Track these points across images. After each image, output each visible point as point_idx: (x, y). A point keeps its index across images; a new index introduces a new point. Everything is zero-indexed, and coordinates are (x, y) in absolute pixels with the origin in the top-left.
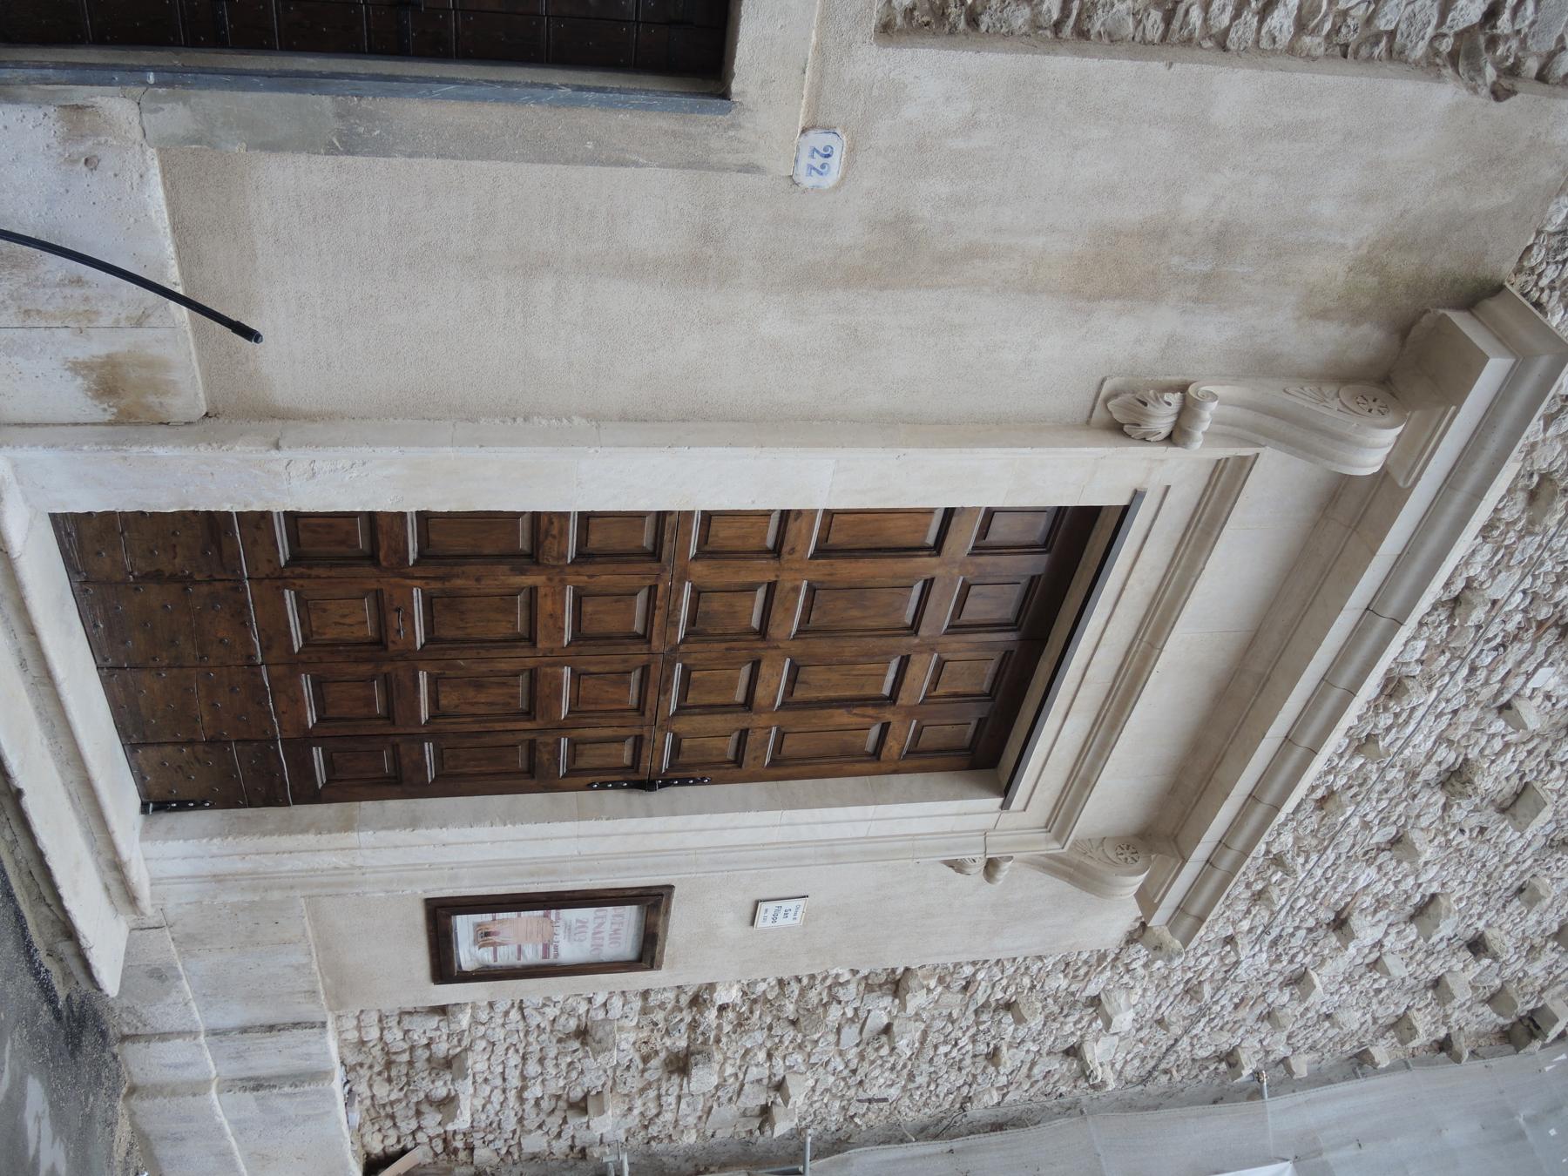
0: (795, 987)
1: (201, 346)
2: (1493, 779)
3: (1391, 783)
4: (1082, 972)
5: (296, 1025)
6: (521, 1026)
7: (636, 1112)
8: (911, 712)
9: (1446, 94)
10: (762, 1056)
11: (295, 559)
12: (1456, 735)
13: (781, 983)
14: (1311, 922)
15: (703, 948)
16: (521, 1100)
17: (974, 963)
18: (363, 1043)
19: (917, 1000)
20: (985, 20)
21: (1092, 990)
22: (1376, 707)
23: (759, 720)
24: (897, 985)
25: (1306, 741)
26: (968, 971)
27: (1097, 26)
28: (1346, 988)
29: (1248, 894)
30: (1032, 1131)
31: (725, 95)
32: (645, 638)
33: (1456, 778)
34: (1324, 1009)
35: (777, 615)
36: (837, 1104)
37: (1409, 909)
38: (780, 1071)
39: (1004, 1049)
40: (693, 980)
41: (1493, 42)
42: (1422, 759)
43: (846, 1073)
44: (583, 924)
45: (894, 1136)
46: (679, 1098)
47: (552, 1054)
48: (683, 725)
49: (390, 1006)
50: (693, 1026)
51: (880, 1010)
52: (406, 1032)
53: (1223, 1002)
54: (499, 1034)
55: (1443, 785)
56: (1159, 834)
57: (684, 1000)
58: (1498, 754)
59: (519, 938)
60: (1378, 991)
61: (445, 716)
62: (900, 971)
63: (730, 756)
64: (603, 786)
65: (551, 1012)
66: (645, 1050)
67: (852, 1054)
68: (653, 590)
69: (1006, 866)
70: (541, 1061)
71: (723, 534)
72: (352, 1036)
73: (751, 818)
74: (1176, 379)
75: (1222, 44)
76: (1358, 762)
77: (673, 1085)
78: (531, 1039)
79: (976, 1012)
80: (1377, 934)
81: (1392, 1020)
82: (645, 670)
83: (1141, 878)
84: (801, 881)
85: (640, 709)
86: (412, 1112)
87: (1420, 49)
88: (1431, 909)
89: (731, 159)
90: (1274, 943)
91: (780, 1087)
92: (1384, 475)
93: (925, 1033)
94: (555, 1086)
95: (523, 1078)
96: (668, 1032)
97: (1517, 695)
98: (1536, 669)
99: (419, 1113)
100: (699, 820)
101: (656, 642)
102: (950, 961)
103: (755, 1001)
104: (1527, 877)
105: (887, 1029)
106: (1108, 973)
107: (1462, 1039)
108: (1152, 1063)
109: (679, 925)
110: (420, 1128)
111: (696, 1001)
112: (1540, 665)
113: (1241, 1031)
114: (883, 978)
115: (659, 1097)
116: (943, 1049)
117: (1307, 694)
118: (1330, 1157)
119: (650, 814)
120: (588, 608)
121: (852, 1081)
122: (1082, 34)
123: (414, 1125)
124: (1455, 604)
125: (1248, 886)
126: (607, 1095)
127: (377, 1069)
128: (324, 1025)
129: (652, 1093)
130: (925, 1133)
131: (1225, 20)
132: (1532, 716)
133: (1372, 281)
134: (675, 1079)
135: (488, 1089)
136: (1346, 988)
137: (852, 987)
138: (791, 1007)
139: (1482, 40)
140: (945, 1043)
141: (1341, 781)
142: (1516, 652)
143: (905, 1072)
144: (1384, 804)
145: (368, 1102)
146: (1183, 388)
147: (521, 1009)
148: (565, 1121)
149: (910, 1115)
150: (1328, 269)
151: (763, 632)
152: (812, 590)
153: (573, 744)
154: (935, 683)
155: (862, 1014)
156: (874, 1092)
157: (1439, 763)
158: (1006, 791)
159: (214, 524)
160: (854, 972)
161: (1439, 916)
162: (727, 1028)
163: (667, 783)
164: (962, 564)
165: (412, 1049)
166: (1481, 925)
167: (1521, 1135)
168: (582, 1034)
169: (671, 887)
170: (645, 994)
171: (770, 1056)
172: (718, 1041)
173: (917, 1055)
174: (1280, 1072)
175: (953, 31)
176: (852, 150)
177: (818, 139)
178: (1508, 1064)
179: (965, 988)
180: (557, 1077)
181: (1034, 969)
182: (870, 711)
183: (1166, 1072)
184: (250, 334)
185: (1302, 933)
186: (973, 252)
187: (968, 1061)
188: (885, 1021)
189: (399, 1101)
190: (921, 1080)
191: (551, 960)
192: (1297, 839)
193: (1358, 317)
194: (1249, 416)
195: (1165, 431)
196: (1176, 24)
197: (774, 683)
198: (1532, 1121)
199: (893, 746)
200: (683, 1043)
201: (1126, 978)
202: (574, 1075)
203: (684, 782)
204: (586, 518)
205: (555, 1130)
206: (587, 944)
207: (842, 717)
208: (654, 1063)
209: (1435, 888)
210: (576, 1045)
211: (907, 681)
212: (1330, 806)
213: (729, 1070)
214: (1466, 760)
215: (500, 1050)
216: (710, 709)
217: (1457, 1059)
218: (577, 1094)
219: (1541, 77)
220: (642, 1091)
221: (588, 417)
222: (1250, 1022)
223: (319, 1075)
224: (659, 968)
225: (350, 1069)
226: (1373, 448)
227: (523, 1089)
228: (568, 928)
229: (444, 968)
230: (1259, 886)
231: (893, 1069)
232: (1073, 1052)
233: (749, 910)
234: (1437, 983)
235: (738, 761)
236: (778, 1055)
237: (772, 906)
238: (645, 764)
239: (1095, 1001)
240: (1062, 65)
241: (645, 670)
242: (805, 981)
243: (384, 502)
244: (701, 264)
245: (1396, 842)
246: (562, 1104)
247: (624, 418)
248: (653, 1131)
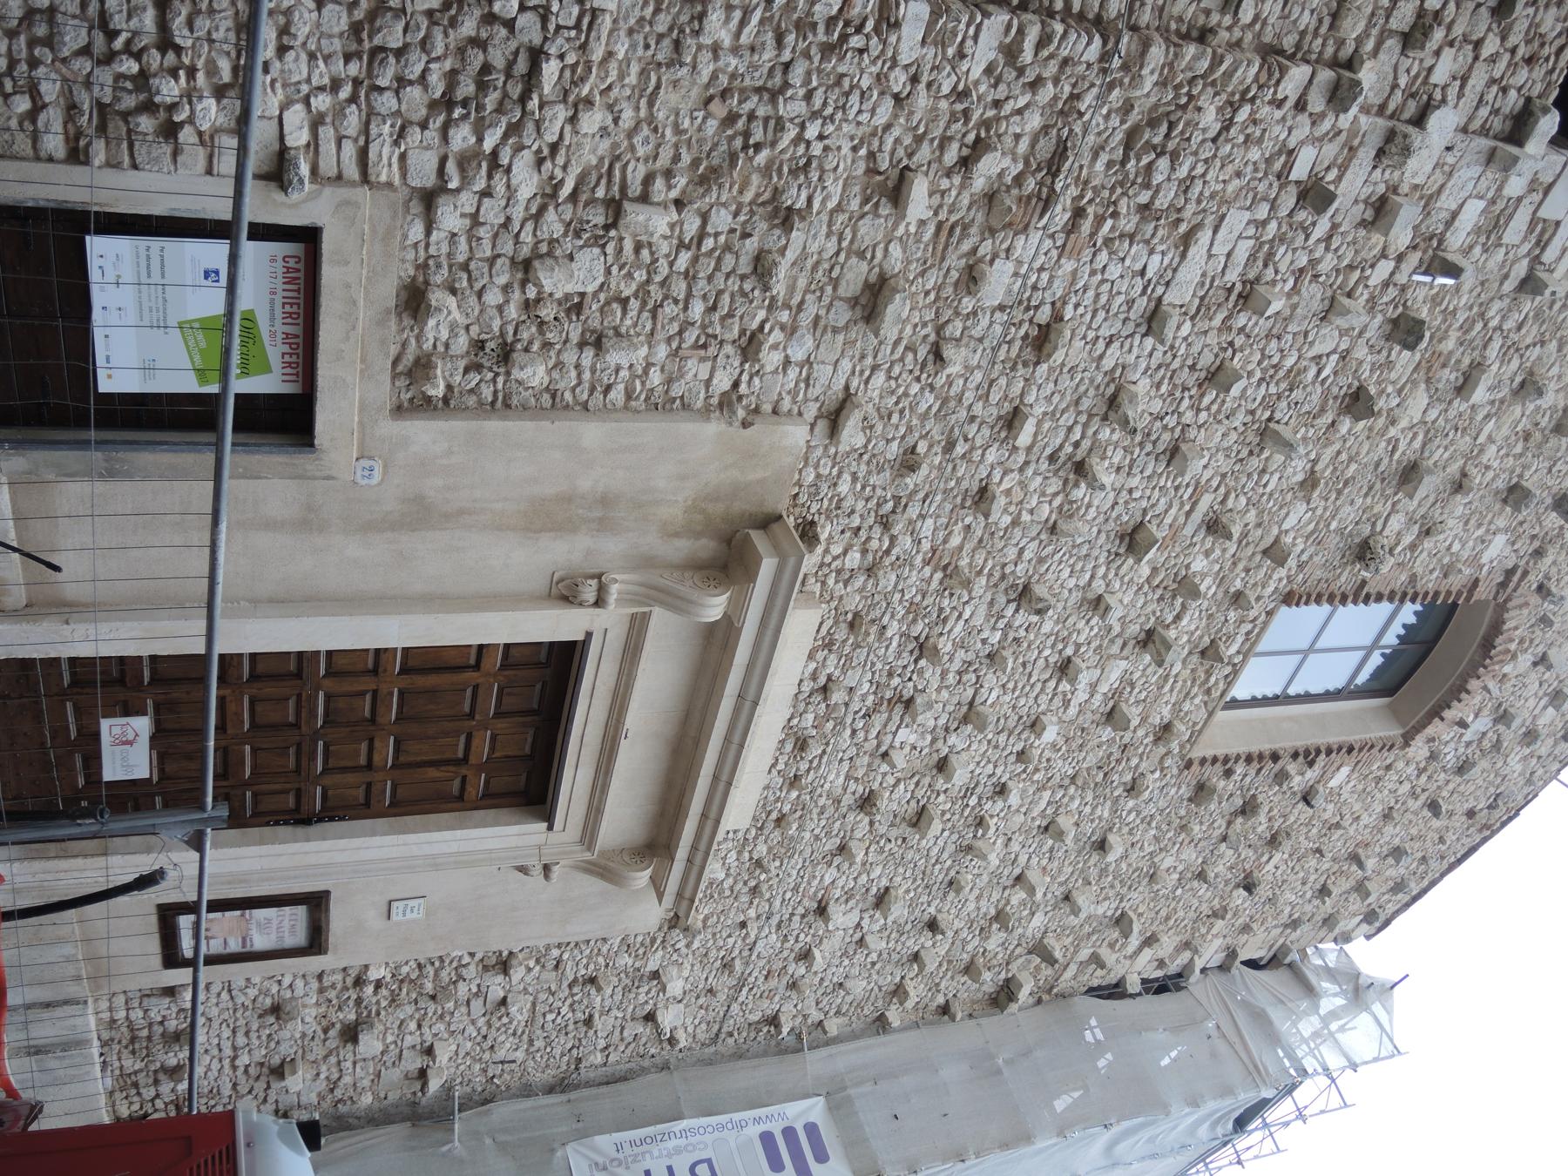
0: (430, 970)
1: (25, 569)
2: (895, 801)
3: (823, 807)
4: (641, 952)
5: (66, 1002)
6: (230, 1005)
7: (322, 1076)
8: (480, 768)
9: (714, 428)
10: (413, 1026)
11: (73, 683)
12: (860, 773)
13: (420, 966)
14: (801, 910)
15: (360, 938)
16: (234, 1068)
17: (559, 946)
18: (113, 1021)
19: (517, 973)
20: (452, 403)
21: (652, 965)
23: (378, 776)
24: (504, 965)
25: (724, 778)
26: (555, 953)
27: (515, 401)
28: (846, 962)
29: (746, 889)
30: (632, 1084)
31: (312, 445)
32: (297, 725)
33: (867, 803)
34: (835, 980)
35: (381, 710)
36: (478, 1067)
37: (871, 899)
38: (429, 1038)
39: (597, 1016)
40: (356, 962)
41: (740, 398)
42: (840, 790)
43: (479, 1039)
44: (269, 921)
45: (527, 1091)
46: (355, 1063)
47: (255, 1027)
48: (328, 780)
49: (133, 985)
50: (359, 1001)
51: (496, 986)
52: (146, 1011)
53: (755, 974)
54: (214, 1012)
55: (861, 807)
56: (656, 845)
57: (349, 981)
58: (894, 786)
59: (223, 932)
60: (873, 964)
61: (169, 778)
62: (505, 954)
63: (362, 801)
64: (277, 823)
65: (252, 992)
66: (324, 1023)
67: (481, 1022)
68: (299, 696)
69: (555, 868)
70: (247, 1034)
71: (340, 662)
72: (106, 1016)
73: (377, 840)
74: (597, 571)
75: (585, 406)
76: (794, 794)
77: (347, 1052)
78: (239, 1014)
79: (570, 986)
80: (854, 918)
81: (893, 988)
82: (299, 745)
83: (648, 872)
84: (417, 885)
85: (298, 770)
86: (151, 1081)
87: (699, 404)
89: (318, 474)
90: (779, 926)
91: (429, 1051)
92: (726, 616)
93: (534, 1004)
94: (259, 1054)
95: (235, 1048)
96: (340, 1008)
97: (891, 746)
99: (156, 1082)
100: (343, 843)
101: (304, 728)
102: (541, 944)
103: (402, 981)
104: (952, 873)
105: (504, 1002)
106: (660, 953)
108: (716, 1027)
109: (338, 920)
110: (157, 1096)
111: (359, 982)
112: (899, 727)
113: (777, 999)
114: (494, 960)
115: (339, 1062)
116: (550, 1017)
118: (852, 1091)
119: (308, 840)
120: (259, 708)
121: (486, 1045)
122: (508, 406)
123: (153, 1093)
125: (745, 883)
126: (299, 1062)
127: (124, 1042)
128: (86, 1002)
129: (333, 1060)
130: (550, 1090)
131: (585, 396)
132: (899, 758)
133: (700, 517)
134: (349, 1046)
135: (208, 1058)
136: (846, 962)
137: (472, 968)
138: (429, 985)
139: (734, 397)
140: (551, 1011)
141: (786, 808)
142: (878, 721)
143: (525, 1037)
144: (823, 822)
145: (117, 1072)
146: (599, 576)
147: (230, 991)
148: (269, 1087)
149: (539, 1077)
150: (674, 512)
151: (373, 720)
152: (401, 693)
153: (255, 795)
154: (492, 749)
155: (484, 990)
156: (501, 1054)
158: (549, 818)
159: (26, 664)
160: (472, 955)
162: (384, 1003)
163: (320, 820)
164: (495, 675)
165: (150, 1025)
166: (932, 910)
167: (999, 1072)
168: (276, 1010)
169: (327, 893)
170: (320, 977)
171: (419, 1026)
172: (378, 1014)
173: (530, 1022)
174: (818, 1033)
175: (435, 408)
176: (385, 466)
177: (366, 463)
178: (993, 1024)
179: (557, 967)
180: (260, 1047)
181: (604, 950)
182: (452, 768)
183: (731, 1034)
184: (57, 569)
185: (797, 919)
186: (461, 512)
187: (571, 1027)
188: (502, 994)
189: (141, 1070)
190: (539, 1044)
191: (248, 949)
192: (770, 849)
193: (698, 535)
194: (630, 587)
195: (592, 600)
196: (558, 400)
197: (387, 751)
198: (1008, 1062)
199: (471, 793)
200: (352, 1017)
201: (675, 957)
202: (273, 1045)
203: (332, 819)
204: (253, 656)
205: (262, 1095)
206: (273, 937)
207: (432, 773)
208: (332, 1033)
209: (884, 882)
210: (272, 1019)
211: (473, 749)
213: (390, 1039)
214: (871, 791)
215: (215, 1024)
216: (344, 770)
218: (276, 1061)
219: (775, 412)
220: (326, 1057)
221: (250, 601)
222: (781, 990)
223: (81, 1043)
224: (326, 953)
225: (105, 1044)
226: (715, 607)
227: (234, 1058)
228: (259, 924)
229: (172, 958)
230: (752, 883)
231: (514, 1034)
232: (650, 1017)
233: (385, 909)
234: (916, 957)
235: (367, 804)
236: (425, 1024)
237: (401, 904)
238: (304, 808)
239: (655, 975)
240: (494, 426)
241: (299, 745)
242: (437, 964)
243: (129, 650)
244: (308, 522)
245: (842, 849)
246: (265, 1070)
247: (271, 601)
248: (338, 1093)
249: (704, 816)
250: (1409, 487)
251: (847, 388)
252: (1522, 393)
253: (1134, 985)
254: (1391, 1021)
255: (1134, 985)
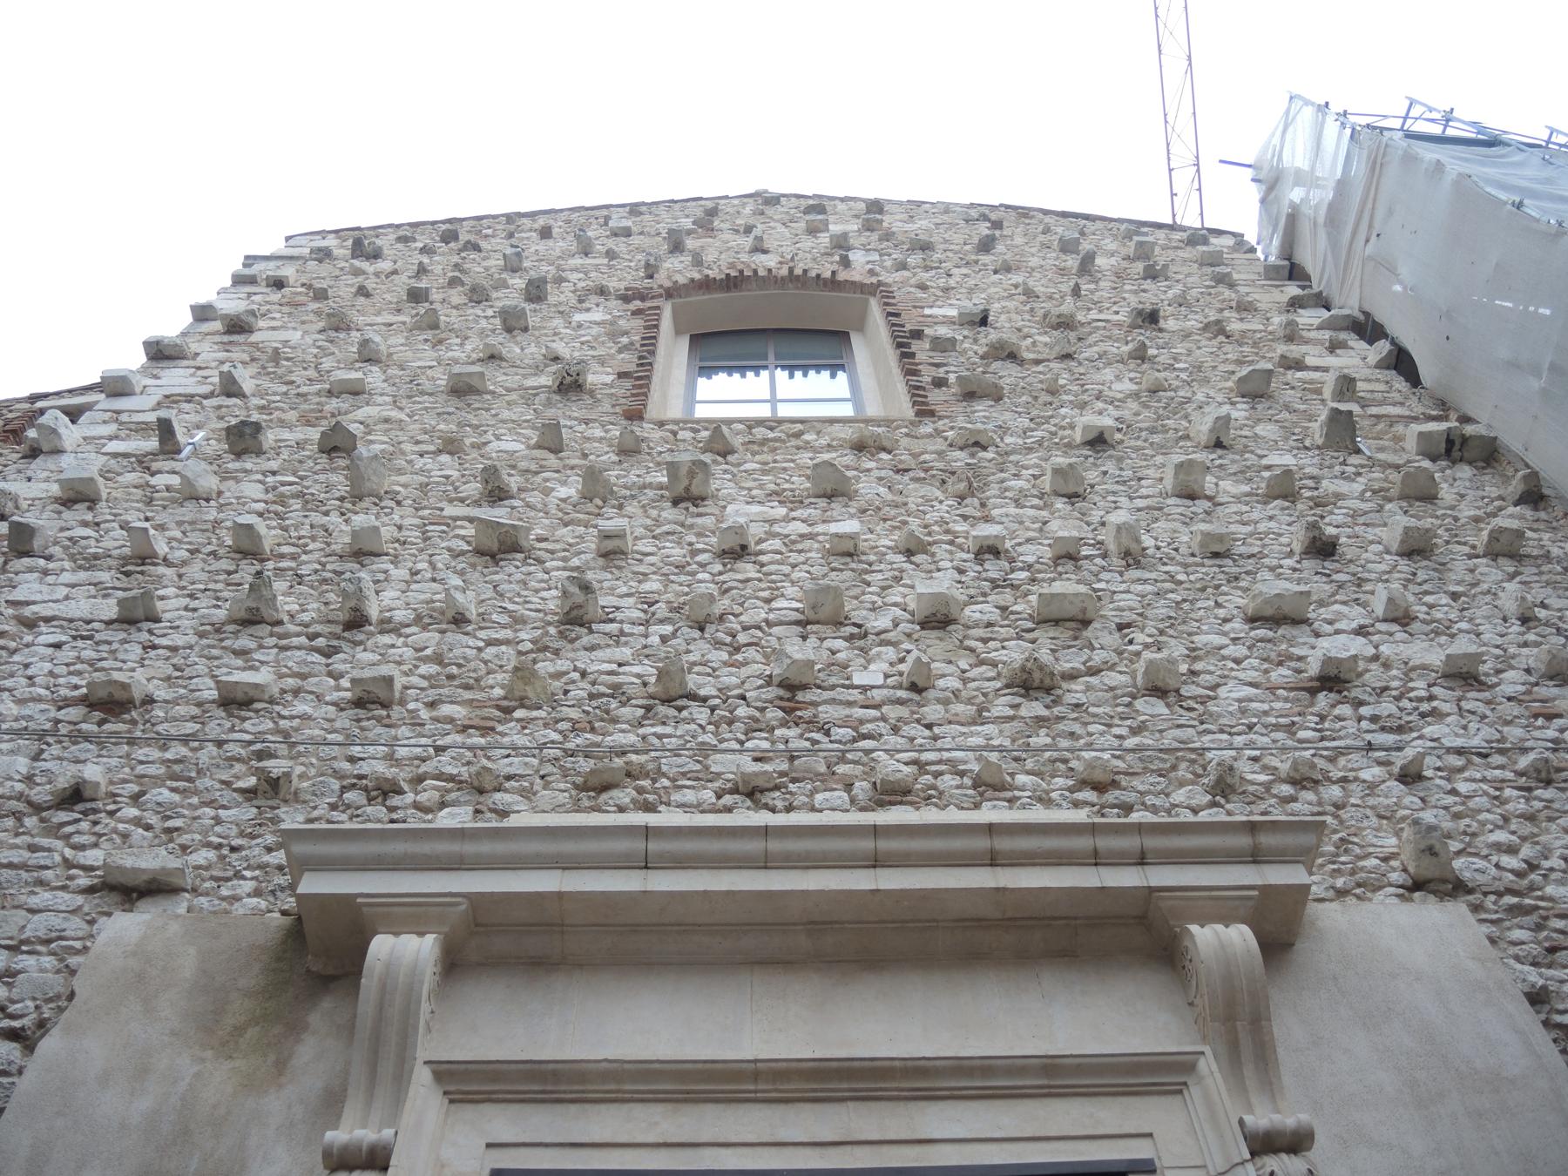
22: (934, 797)
25: (867, 844)
56: (1139, 938)
83: (1194, 928)
88: (1269, 612)
98: (857, 687)
106: (1550, 890)
107: (1510, 489)
117: (358, 876)
124: (752, 792)
157: (1016, 707)
161: (1266, 602)
212: (1099, 776)
214: (1007, 686)
217: (1533, 477)
249: (993, 860)
250: (475, 382)
251: (90, 890)
252: (373, 356)
253: (1383, 347)
254: (1273, 134)
255: (1383, 347)
